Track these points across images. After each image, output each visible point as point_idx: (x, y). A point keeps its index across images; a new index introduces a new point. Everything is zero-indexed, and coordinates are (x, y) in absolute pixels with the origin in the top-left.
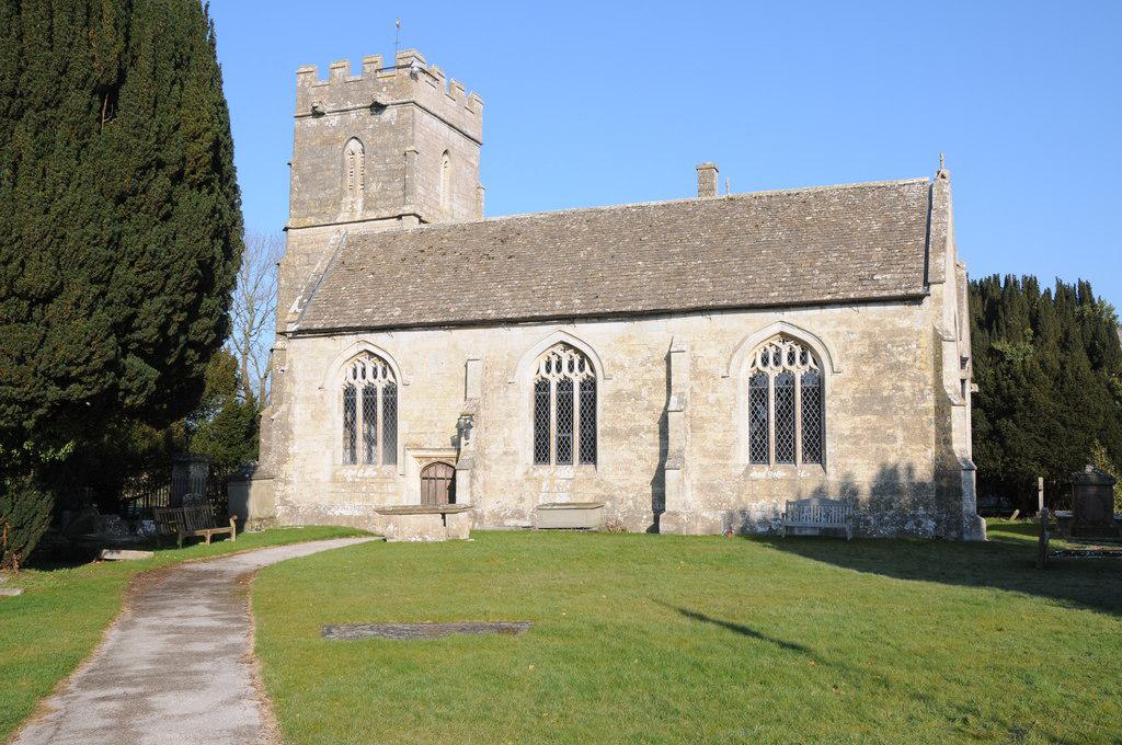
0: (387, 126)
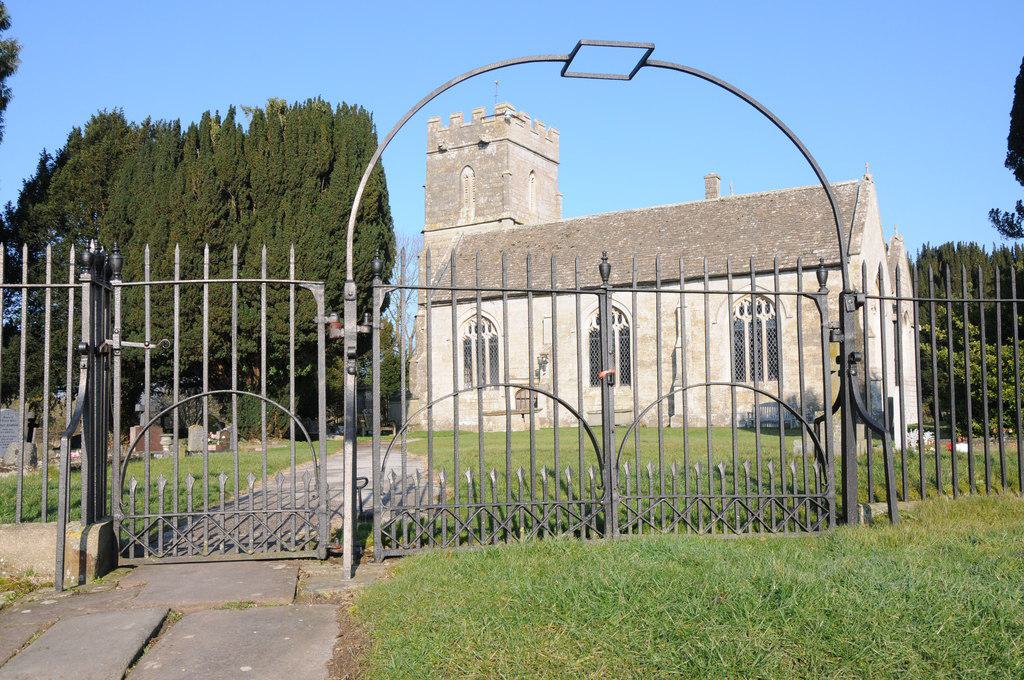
0: (490, 156)
